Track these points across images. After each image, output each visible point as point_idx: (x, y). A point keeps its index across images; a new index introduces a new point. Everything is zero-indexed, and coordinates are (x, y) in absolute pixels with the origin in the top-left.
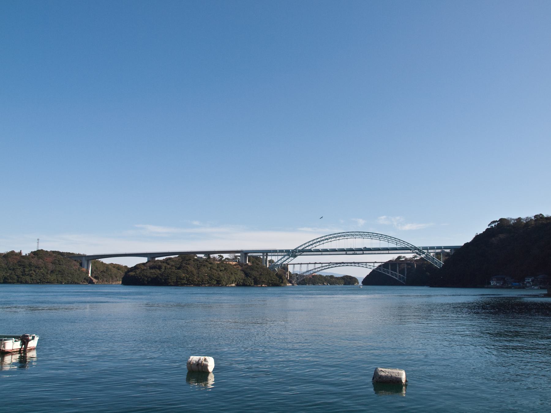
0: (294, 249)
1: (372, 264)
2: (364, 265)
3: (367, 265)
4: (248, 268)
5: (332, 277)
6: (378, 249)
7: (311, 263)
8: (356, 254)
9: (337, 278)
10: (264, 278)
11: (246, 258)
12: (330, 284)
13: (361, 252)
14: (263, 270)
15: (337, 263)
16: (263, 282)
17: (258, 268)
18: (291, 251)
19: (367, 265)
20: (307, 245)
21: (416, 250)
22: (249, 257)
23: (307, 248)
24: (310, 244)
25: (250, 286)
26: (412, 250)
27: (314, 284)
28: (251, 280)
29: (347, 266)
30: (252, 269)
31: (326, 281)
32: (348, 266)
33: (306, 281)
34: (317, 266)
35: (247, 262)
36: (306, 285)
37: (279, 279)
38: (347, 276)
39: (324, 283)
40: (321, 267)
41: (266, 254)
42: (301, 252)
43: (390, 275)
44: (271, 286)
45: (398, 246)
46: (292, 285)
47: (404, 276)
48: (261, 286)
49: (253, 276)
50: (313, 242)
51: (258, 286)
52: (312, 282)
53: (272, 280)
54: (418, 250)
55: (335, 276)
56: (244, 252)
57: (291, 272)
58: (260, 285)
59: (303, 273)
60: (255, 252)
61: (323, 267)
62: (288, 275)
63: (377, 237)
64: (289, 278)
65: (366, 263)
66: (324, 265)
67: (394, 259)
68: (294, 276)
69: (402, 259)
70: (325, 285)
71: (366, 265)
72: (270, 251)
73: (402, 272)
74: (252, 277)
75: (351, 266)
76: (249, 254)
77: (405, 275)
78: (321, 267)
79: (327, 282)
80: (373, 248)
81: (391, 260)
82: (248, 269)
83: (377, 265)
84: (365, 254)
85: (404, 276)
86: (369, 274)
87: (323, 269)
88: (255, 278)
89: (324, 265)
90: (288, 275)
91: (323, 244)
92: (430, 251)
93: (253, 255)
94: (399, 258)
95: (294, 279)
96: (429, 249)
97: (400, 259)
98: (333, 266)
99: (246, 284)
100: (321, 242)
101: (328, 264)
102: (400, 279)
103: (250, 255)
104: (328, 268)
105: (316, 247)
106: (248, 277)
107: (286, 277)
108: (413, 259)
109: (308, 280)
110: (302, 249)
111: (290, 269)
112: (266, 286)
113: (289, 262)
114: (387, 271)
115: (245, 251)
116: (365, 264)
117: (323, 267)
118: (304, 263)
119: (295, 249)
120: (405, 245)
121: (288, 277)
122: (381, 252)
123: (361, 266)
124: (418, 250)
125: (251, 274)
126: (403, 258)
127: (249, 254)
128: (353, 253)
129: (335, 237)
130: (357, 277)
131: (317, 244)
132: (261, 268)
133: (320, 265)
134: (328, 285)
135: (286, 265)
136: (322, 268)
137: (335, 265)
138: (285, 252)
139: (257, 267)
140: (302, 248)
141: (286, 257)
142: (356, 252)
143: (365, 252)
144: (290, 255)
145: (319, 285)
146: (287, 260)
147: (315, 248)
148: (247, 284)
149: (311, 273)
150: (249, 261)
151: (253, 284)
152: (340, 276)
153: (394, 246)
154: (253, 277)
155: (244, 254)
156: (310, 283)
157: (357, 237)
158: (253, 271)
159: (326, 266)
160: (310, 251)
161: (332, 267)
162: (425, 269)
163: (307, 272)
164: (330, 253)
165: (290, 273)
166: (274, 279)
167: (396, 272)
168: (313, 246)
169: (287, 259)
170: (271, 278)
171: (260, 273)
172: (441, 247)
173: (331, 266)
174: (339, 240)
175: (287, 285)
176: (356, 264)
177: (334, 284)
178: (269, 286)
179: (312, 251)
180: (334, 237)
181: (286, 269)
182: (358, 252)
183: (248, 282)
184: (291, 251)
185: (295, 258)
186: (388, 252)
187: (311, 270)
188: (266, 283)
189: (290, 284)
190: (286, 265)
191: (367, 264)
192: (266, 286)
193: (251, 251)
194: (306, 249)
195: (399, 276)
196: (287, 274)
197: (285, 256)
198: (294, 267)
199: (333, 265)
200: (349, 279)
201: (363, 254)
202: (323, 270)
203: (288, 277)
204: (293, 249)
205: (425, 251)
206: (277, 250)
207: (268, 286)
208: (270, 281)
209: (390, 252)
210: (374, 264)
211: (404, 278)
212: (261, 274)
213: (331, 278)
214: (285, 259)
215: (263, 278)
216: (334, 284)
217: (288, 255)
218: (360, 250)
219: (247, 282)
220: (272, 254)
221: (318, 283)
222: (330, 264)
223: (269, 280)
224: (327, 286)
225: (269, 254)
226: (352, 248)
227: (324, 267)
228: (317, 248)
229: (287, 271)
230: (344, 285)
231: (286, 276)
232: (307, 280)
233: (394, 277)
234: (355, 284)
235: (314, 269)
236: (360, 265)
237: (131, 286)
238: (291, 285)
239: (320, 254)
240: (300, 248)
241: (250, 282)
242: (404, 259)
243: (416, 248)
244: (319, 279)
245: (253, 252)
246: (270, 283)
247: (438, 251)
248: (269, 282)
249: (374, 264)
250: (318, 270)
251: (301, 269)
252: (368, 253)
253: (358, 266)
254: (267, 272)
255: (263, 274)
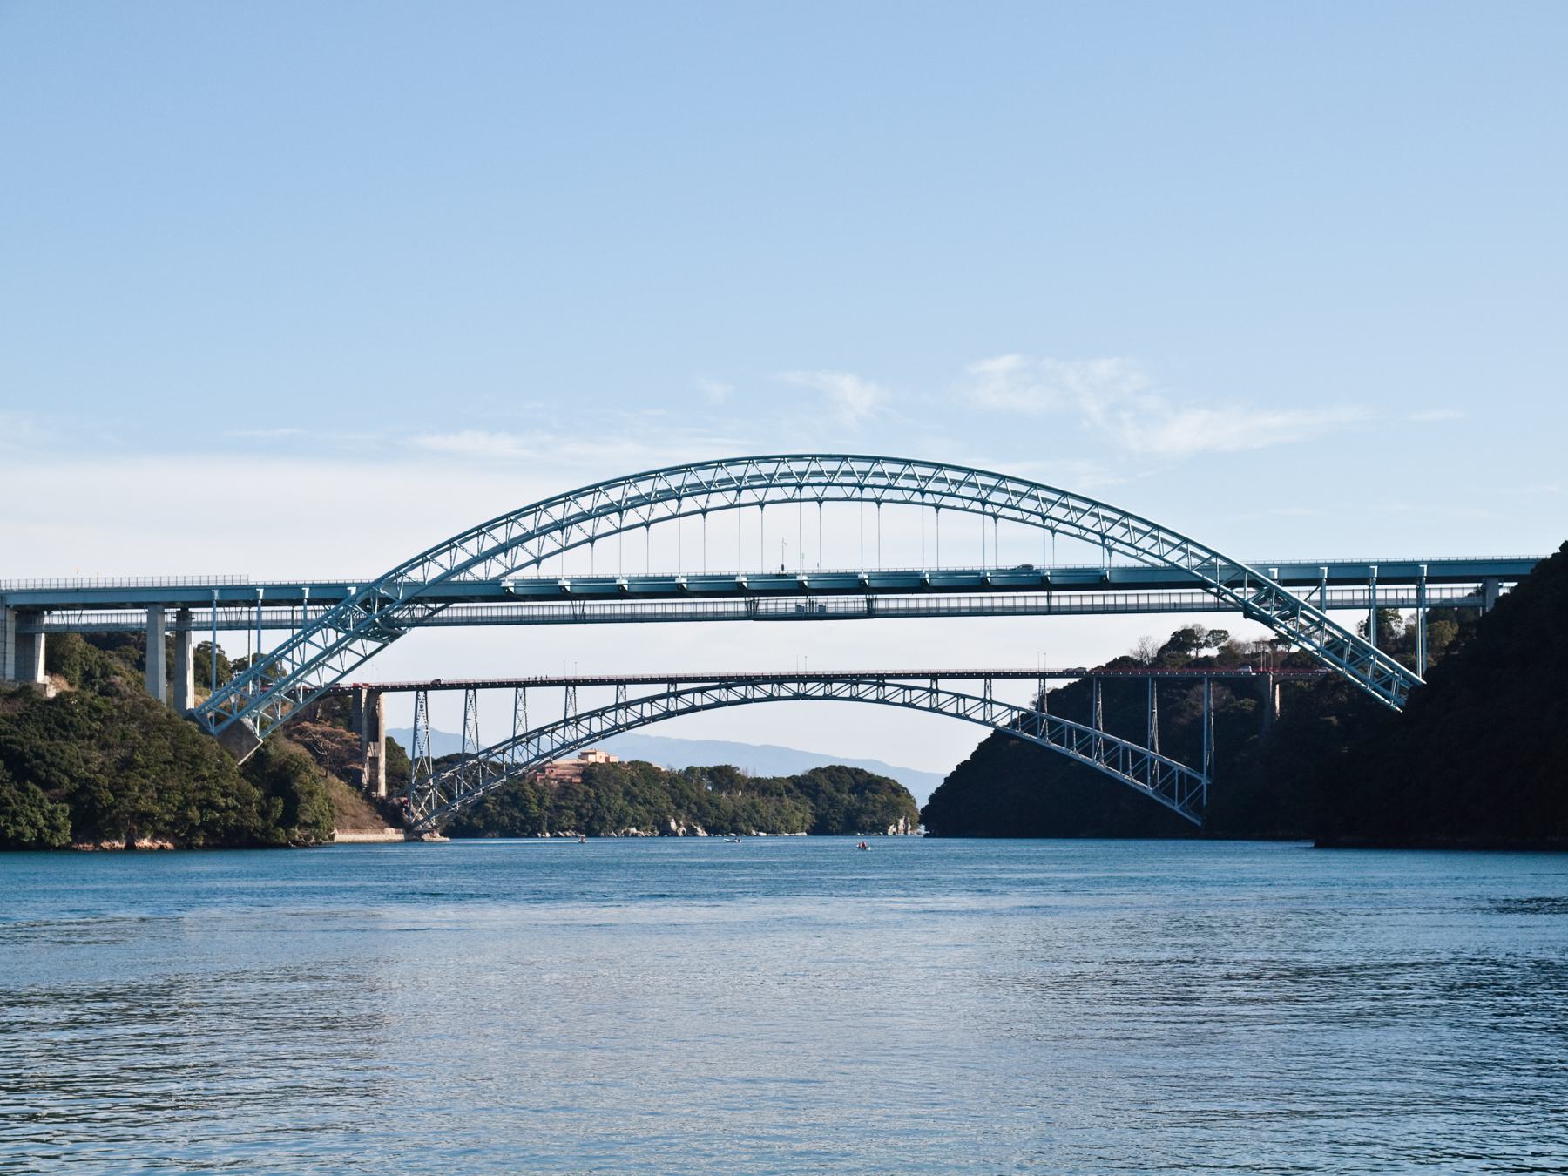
0: (378, 582)
1: (975, 687)
2: (916, 693)
3: (937, 691)
4: (24, 718)
5: (723, 776)
6: (976, 582)
7: (445, 679)
8: (823, 615)
9: (764, 787)
10: (152, 792)
11: (25, 643)
12: (708, 829)
13: (857, 602)
14: (146, 734)
15: (726, 682)
16: (144, 821)
17: (111, 718)
18: (353, 590)
19: (937, 691)
20: (472, 547)
21: (1240, 584)
22: (57, 638)
23: (478, 572)
24: (545, 520)
25: (41, 846)
26: (1212, 586)
27: (591, 833)
28: (50, 807)
29: (797, 697)
30: (65, 727)
31: (680, 807)
32: (805, 697)
33: (535, 810)
34: (590, 699)
35: (41, 677)
36: (533, 834)
37: (267, 796)
38: (837, 774)
39: (667, 823)
40: (617, 707)
41: (179, 616)
42: (435, 600)
43: (1101, 765)
44: (199, 848)
45: (1120, 561)
46: (407, 841)
47: (1199, 769)
48: (131, 848)
49: (66, 772)
50: (574, 510)
51: (105, 844)
52: (580, 816)
53: (212, 805)
54: (1255, 583)
55: (754, 768)
56: (12, 601)
57: (400, 742)
58: (118, 838)
59: (489, 750)
60: (90, 600)
61: (628, 705)
62: (382, 764)
63: (972, 492)
64: (388, 785)
65: (934, 677)
66: (634, 692)
67: (1149, 649)
68: (422, 770)
69: (1204, 652)
70: (675, 834)
71: (931, 691)
72: (203, 596)
73: (1181, 741)
74: (60, 785)
75: (851, 699)
76: (54, 619)
77: (1206, 762)
78: (617, 707)
79: (689, 811)
80: (936, 574)
81: (1124, 659)
82: (30, 727)
83: (1024, 695)
84: (887, 614)
85: (1199, 769)
86: (974, 755)
87: (631, 719)
88: (83, 789)
89: (634, 692)
90: (382, 764)
91: (592, 540)
92: (1335, 593)
93: (123, 620)
94: (1184, 639)
95: (422, 793)
96: (1431, 580)
97: (1193, 653)
98: (699, 700)
99: (11, 833)
100: (685, 501)
101: (662, 688)
102: (1167, 791)
103: (56, 621)
104: (668, 714)
105: (538, 561)
106: (31, 786)
107: (365, 780)
108: (1280, 648)
109: (548, 802)
110: (436, 582)
111: (395, 715)
112: (168, 845)
113: (344, 674)
114: (1081, 734)
115: (21, 592)
116: (926, 683)
117: (628, 705)
118: (596, 675)
119: (387, 580)
120: (1167, 548)
121: (382, 777)
122: (998, 603)
123: (899, 700)
124: (1255, 583)
125: (52, 764)
126: (1207, 644)
127: (54, 619)
128: (799, 607)
129: (730, 480)
130: (906, 771)
131: (550, 543)
132: (132, 719)
133: (607, 695)
134: (692, 832)
135: (364, 693)
136: (622, 717)
137: (715, 693)
138: (310, 602)
139: (98, 710)
140: (433, 571)
141: (317, 638)
142: (821, 600)
143: (883, 602)
144: (345, 625)
145: (626, 834)
146: (334, 662)
147: (531, 573)
148: (21, 835)
149: (546, 747)
150: (51, 669)
151: (65, 836)
152: (785, 772)
153: (1089, 557)
154: (66, 780)
155: (11, 618)
156: (565, 823)
157: (831, 492)
158: (67, 739)
159: (652, 700)
160: (494, 592)
161: (693, 709)
162: (1333, 719)
163: (515, 741)
164: (638, 610)
165: (393, 749)
166: (225, 795)
167: (1141, 738)
168: (521, 555)
169: (329, 652)
170: (203, 788)
171: (123, 752)
172: (1414, 565)
173: (689, 697)
174: (647, 524)
175: (339, 837)
176: (862, 687)
177: (742, 826)
178: (185, 846)
179: (507, 596)
180: (725, 485)
181: (365, 723)
182: (832, 603)
183: (33, 825)
184: (353, 590)
185: (393, 646)
186: (1043, 602)
187: (541, 731)
188: (160, 826)
189: (392, 834)
190: (364, 693)
191: (943, 684)
192: (168, 845)
193: (106, 591)
194: (467, 577)
195: (1165, 768)
196: (375, 760)
197: (308, 628)
198: (421, 708)
199: (702, 691)
200: (852, 791)
201: (871, 613)
202: (654, 719)
203: (382, 777)
204: (371, 575)
205: (1301, 598)
206: (252, 589)
207: (178, 848)
208: (194, 814)
209: (1062, 598)
210: (988, 688)
211: (1193, 782)
212: (127, 764)
213: (719, 787)
214: (311, 652)
215: (143, 789)
216: (738, 831)
217: (338, 623)
218: (849, 584)
219: (20, 819)
220: (221, 618)
221: (620, 823)
222: (681, 687)
223: (187, 803)
224: (692, 841)
225: (201, 615)
226: (789, 570)
227: (637, 708)
228: (550, 570)
229: (375, 737)
230: (808, 832)
231: (360, 773)
232: (540, 803)
233: (1128, 778)
234: (892, 829)
235: (566, 722)
236: (888, 690)
237: (1276, 846)
238: (401, 837)
239: (567, 611)
240: (416, 575)
241: (42, 822)
242: (1212, 652)
243: (1237, 576)
244: (630, 797)
245: (79, 599)
246: (193, 830)
247: (1446, 595)
248: (186, 819)
249: (988, 688)
250: (570, 739)
251: (471, 723)
252: (902, 605)
253: (873, 696)
254: (177, 748)
255: (139, 758)
